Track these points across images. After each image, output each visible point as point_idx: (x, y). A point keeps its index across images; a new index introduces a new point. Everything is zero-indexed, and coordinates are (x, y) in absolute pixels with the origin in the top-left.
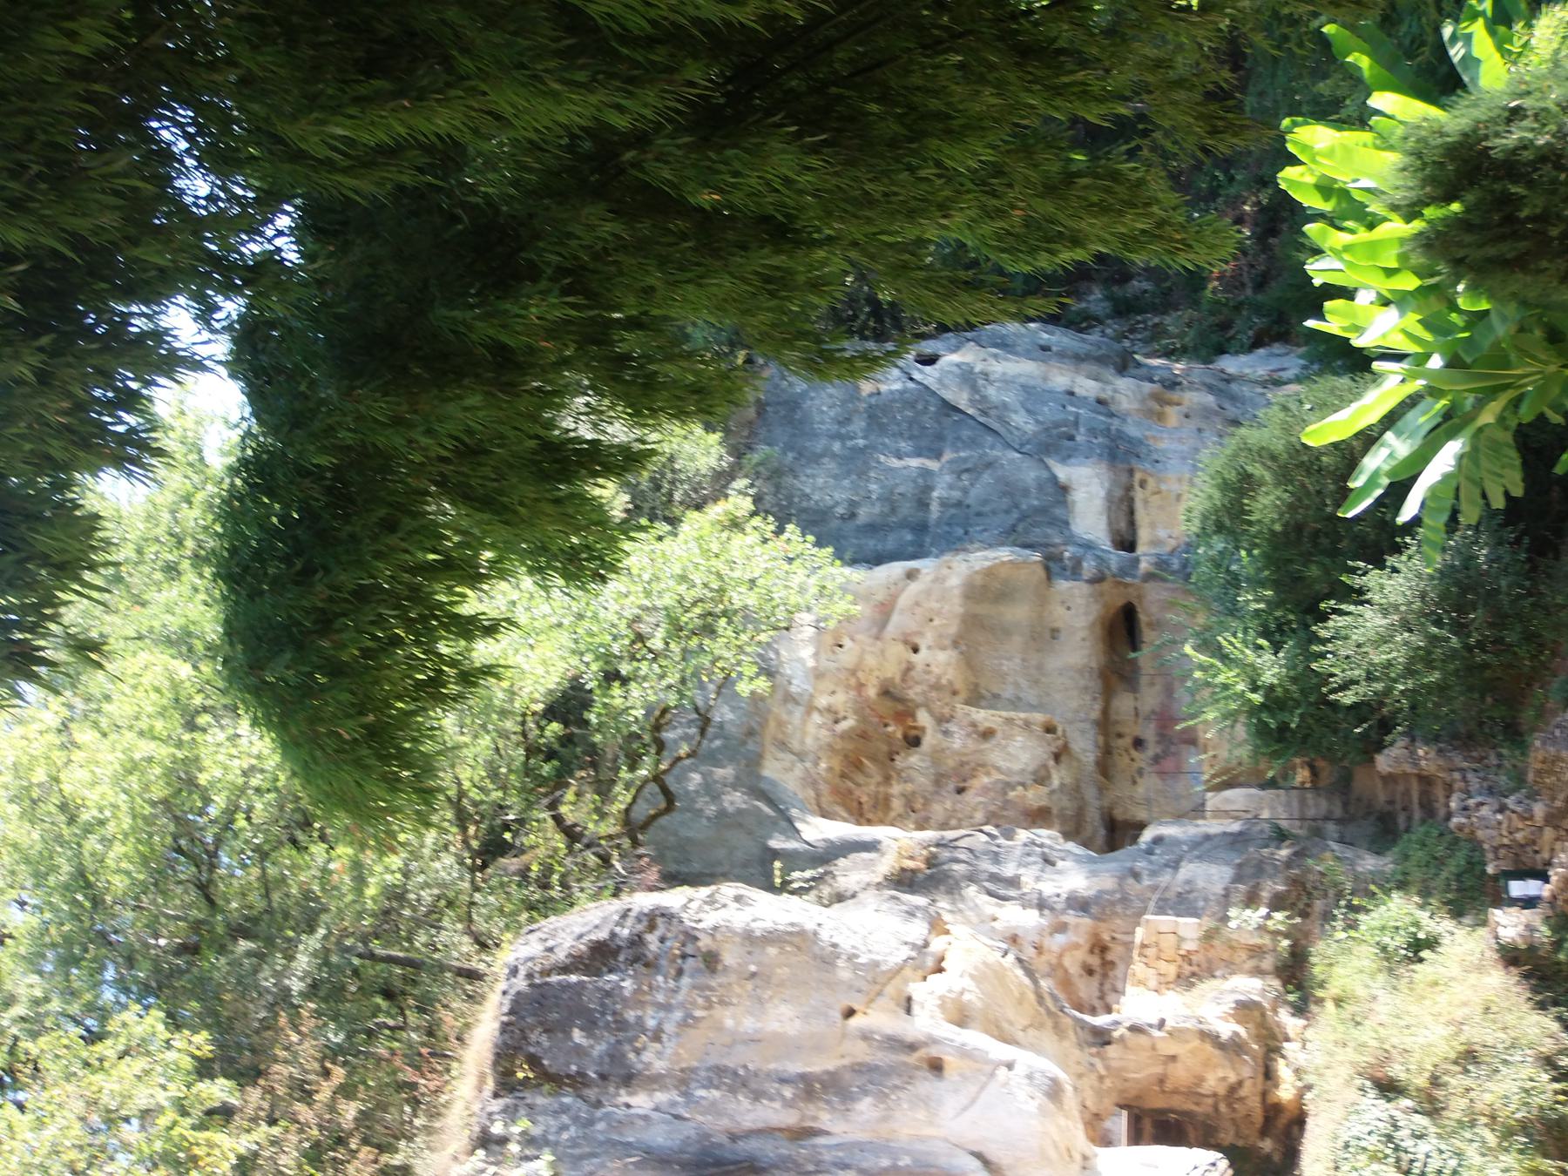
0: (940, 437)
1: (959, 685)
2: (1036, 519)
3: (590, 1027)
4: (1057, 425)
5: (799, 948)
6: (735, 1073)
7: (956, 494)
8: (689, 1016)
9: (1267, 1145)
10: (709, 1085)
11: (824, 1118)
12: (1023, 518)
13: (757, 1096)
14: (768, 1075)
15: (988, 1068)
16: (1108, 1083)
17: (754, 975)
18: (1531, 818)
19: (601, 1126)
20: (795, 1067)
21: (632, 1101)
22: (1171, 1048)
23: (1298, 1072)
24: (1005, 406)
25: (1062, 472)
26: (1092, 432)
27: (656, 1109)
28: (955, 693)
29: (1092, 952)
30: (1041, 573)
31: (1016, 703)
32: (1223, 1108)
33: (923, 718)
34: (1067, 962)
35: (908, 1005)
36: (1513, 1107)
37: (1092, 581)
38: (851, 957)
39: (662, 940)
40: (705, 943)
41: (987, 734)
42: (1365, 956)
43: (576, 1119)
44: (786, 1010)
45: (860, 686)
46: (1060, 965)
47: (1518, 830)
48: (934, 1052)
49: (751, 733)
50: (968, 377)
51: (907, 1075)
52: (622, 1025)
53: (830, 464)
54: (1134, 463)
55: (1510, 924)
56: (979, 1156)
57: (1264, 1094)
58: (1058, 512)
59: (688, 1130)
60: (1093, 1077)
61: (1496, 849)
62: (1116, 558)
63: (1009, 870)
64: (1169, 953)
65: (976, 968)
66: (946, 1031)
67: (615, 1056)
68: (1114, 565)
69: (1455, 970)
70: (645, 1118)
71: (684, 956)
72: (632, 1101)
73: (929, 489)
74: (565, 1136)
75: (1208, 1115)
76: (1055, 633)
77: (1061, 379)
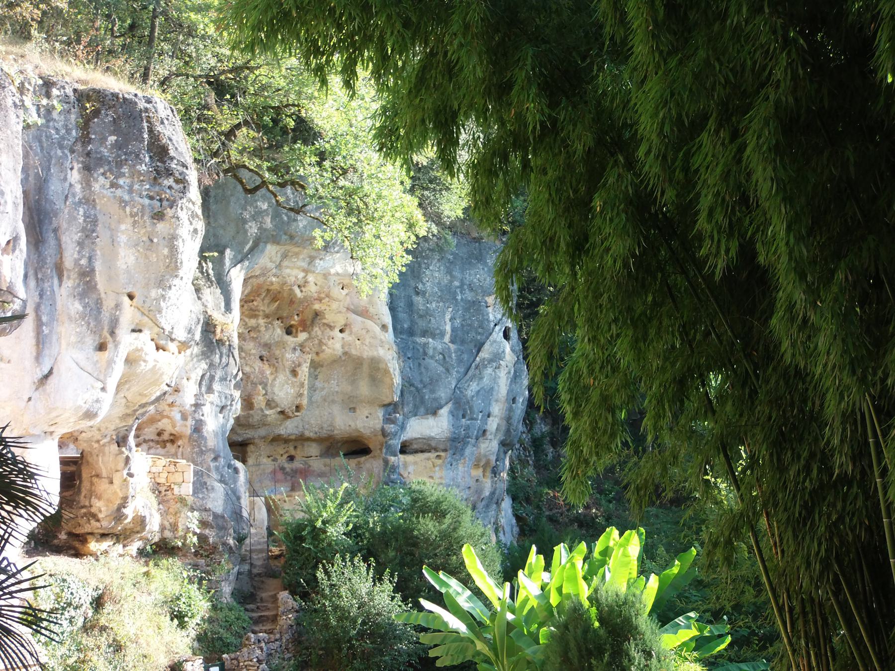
0: (463, 342)
1: (322, 356)
2: (417, 397)
3: (118, 146)
4: (471, 408)
6: (93, 231)
7: (431, 352)
8: (126, 203)
9: (63, 536)
10: (86, 216)
13: (80, 244)
14: (93, 250)
15: (102, 378)
16: (96, 445)
17: (152, 241)
19: (59, 152)
20: (98, 266)
21: (75, 171)
24: (481, 378)
25: (444, 411)
26: (467, 428)
27: (71, 185)
29: (171, 435)
30: (387, 401)
31: (312, 389)
32: (84, 510)
33: (303, 336)
34: (165, 421)
37: (383, 430)
39: (170, 187)
40: (169, 212)
41: (294, 373)
42: (174, 588)
44: (131, 260)
45: (320, 300)
46: (163, 417)
48: (110, 346)
49: (292, 237)
50: (497, 357)
51: (96, 331)
52: (120, 164)
53: (446, 280)
57: (92, 534)
58: (422, 410)
59: (59, 204)
60: (99, 437)
61: (236, 659)
62: (397, 443)
63: (216, 386)
64: (172, 479)
67: (101, 161)
70: (65, 179)
71: (161, 200)
72: (75, 171)
73: (433, 336)
75: (79, 502)
76: (353, 410)
77: (497, 409)
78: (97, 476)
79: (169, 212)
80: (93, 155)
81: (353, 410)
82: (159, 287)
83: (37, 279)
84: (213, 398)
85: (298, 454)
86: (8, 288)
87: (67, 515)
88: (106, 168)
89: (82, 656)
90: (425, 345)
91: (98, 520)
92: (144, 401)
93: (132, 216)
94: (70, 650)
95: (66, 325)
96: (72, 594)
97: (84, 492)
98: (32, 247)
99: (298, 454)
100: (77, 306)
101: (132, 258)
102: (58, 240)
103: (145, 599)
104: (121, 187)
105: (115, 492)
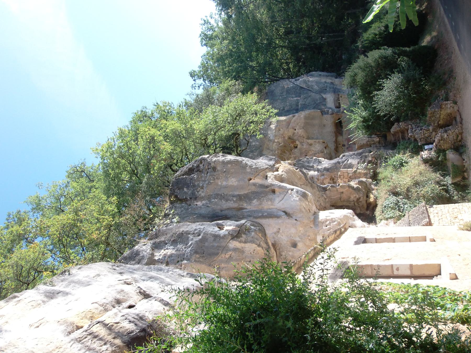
0: (300, 93)
1: (304, 136)
2: (319, 105)
3: (188, 187)
4: (323, 88)
6: (221, 195)
7: (304, 103)
8: (209, 182)
9: (368, 212)
10: (215, 198)
11: (245, 205)
13: (227, 200)
14: (230, 195)
16: (327, 200)
17: (225, 171)
18: (429, 130)
19: (189, 210)
20: (237, 193)
22: (342, 190)
24: (312, 85)
25: (324, 96)
26: (330, 88)
27: (203, 205)
28: (304, 137)
29: (330, 180)
31: (317, 139)
32: (356, 204)
33: (297, 142)
36: (429, 194)
37: (331, 114)
38: (251, 167)
39: (203, 165)
40: (212, 165)
41: (311, 145)
42: (390, 169)
43: (185, 209)
44: (233, 180)
45: (284, 137)
47: (426, 134)
48: (273, 188)
49: (261, 146)
50: (305, 82)
51: (266, 194)
52: (194, 186)
54: (339, 93)
56: (284, 212)
57: (366, 201)
58: (324, 103)
59: (210, 209)
60: (323, 198)
61: (420, 139)
62: (336, 110)
63: (311, 165)
64: (346, 176)
66: (277, 183)
67: (193, 193)
70: (200, 207)
73: (298, 103)
74: (182, 212)
76: (324, 126)
77: (323, 80)
78: (340, 199)
79: (212, 165)
84: (315, 166)
85: (342, 143)
86: (238, 227)
88: (195, 191)
92: (304, 179)
93: (214, 180)
95: (263, 206)
96: (391, 203)
101: (233, 179)
104: (203, 185)
105: (347, 191)
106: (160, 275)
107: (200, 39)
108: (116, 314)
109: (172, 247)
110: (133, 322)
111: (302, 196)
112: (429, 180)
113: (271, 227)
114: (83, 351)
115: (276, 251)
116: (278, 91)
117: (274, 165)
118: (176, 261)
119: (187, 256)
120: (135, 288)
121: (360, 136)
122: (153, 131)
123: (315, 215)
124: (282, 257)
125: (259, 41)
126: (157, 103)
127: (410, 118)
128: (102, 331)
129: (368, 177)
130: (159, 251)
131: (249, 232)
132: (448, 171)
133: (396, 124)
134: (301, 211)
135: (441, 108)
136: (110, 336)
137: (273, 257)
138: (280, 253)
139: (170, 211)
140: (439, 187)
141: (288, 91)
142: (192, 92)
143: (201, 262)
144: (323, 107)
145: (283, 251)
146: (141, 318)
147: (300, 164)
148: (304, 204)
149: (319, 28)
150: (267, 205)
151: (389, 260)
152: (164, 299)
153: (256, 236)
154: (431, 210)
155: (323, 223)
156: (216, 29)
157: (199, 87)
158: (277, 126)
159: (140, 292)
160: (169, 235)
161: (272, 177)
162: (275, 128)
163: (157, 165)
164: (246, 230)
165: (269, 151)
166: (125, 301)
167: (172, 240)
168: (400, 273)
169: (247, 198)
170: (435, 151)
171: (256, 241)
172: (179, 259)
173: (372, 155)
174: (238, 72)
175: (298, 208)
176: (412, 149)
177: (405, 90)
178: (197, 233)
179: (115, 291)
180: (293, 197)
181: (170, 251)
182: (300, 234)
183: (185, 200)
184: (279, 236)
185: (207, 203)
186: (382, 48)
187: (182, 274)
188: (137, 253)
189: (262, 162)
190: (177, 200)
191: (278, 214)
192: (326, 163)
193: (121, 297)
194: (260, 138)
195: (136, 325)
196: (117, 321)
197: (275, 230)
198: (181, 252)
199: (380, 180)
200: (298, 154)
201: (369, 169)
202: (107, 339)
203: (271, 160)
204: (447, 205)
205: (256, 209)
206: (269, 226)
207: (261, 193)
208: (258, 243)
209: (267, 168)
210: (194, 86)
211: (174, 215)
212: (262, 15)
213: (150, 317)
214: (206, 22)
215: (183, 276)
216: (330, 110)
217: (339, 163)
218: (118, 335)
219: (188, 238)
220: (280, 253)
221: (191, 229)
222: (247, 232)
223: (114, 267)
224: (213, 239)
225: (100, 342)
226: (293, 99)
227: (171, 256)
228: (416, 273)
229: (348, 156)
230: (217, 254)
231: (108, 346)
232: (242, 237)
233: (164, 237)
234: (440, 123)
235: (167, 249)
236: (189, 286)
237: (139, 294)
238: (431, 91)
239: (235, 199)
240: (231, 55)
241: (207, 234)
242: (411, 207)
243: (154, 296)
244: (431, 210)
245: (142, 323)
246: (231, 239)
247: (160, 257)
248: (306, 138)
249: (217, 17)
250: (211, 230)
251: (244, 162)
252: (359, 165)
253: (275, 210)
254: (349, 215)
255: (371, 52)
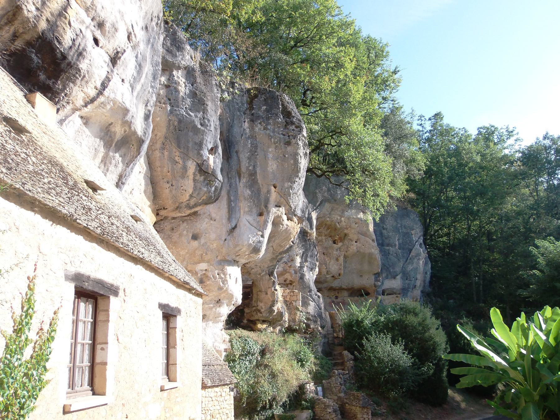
0: (403, 249)
1: (348, 252)
2: (388, 270)
3: (267, 111)
4: (409, 276)
5: (293, 170)
6: (256, 152)
7: (391, 253)
9: (245, 321)
11: (244, 180)
12: (388, 268)
13: (249, 158)
14: (256, 162)
15: (261, 229)
16: (259, 276)
19: (238, 113)
20: (258, 170)
21: (246, 124)
23: (265, 329)
24: (413, 264)
26: (409, 284)
28: (346, 252)
30: (376, 272)
31: (345, 267)
32: (254, 308)
33: (340, 244)
34: (288, 274)
35: (278, 206)
38: (291, 187)
39: (293, 130)
40: (293, 141)
41: (337, 260)
42: (297, 348)
46: (287, 272)
48: (265, 213)
49: (335, 201)
50: (418, 255)
52: (268, 119)
53: (395, 224)
55: (311, 387)
56: (236, 226)
57: (258, 320)
58: (390, 276)
59: (238, 138)
60: (260, 272)
61: (330, 383)
62: (380, 290)
63: (309, 259)
64: (292, 298)
65: (289, 230)
66: (271, 218)
67: (259, 117)
68: (379, 290)
69: (296, 372)
70: (241, 126)
71: (289, 136)
72: (246, 123)
74: (235, 104)
75: (252, 304)
76: (361, 276)
77: (419, 277)
78: (260, 291)
79: (293, 141)
80: (255, 115)
81: (361, 276)
82: (289, 181)
83: (228, 177)
85: (339, 295)
87: (247, 310)
88: (261, 120)
89: (256, 380)
90: (388, 250)
91: (261, 313)
92: (281, 250)
93: (275, 143)
94: (250, 377)
96: (250, 347)
97: (254, 299)
98: (225, 157)
99: (339, 295)
100: (248, 192)
101: (275, 166)
102: (238, 157)
103: (284, 352)
106: (146, 77)
107: (488, 125)
108: (83, 22)
109: (188, 92)
110: (74, 44)
111: (255, 247)
112: (278, 389)
113: (217, 211)
114: (316, 6)
115: (188, 215)
116: (407, 222)
117: (295, 215)
118: (170, 97)
119: (176, 110)
120: (123, 46)
121: (342, 317)
122: (350, 66)
123: (235, 262)
124: (181, 222)
125: (478, 199)
126: (398, 71)
127: (358, 373)
128: (56, 5)
129: (291, 323)
130: (184, 76)
131: (207, 184)
132: (289, 411)
133: (352, 357)
134: (237, 245)
135: (363, 407)
136: (49, 15)
137: (180, 212)
138: (186, 220)
139: (238, 89)
140: (269, 400)
141: (407, 235)
142: (415, 116)
143: (168, 127)
144: (384, 275)
145: (188, 224)
146: (80, 54)
147: (310, 246)
148: (244, 249)
149: (492, 273)
150: (244, 206)
151: (118, 340)
152: (110, 83)
153: (202, 193)
154: (226, 389)
155: (222, 270)
156: (499, 146)
157: (421, 125)
158: (361, 220)
159: (118, 52)
160: (203, 88)
161: (280, 213)
162: (358, 218)
163: (302, 72)
164: (210, 181)
165: (330, 210)
166: (103, 34)
167: (197, 92)
168: (98, 352)
169: (253, 183)
170: (313, 398)
171: (196, 193)
172: (172, 101)
173: (317, 328)
174: (436, 174)
175: (240, 243)
176: (320, 373)
177: (389, 369)
178: (205, 122)
179: (115, 21)
180: (257, 238)
181: (183, 88)
182: (208, 244)
183: (251, 108)
184: (206, 220)
185: (246, 134)
186: (448, 346)
187: (148, 105)
188: (180, 48)
189: (299, 200)
190: (252, 98)
191: (234, 219)
192: (311, 277)
193: (107, 29)
194: (345, 200)
195: (71, 47)
196: (72, 24)
197: (214, 215)
198: (181, 102)
199: (284, 336)
200: (326, 244)
201: (299, 325)
202: (45, 12)
203: (303, 212)
204: (233, 407)
205: (239, 193)
206: (219, 208)
207: (259, 200)
208: (194, 195)
209: (291, 207)
210: (423, 118)
211: (233, 94)
212: (510, 204)
213: (83, 65)
214: (510, 133)
215: (146, 106)
216: (379, 283)
217: (310, 291)
218: (53, 26)
219: (199, 112)
220: (186, 220)
221: (210, 115)
222: (206, 182)
223: (154, 19)
224: (197, 142)
225: (40, 3)
226: (396, 240)
227: (177, 91)
228: (97, 369)
229: (318, 302)
230: (179, 146)
231: (35, 13)
232: (201, 176)
233: (202, 82)
234: (347, 405)
235: (186, 86)
236: (131, 113)
237: (115, 51)
238: (388, 398)
239: (250, 168)
240: (460, 165)
241: (203, 135)
242: (246, 368)
243: (115, 70)
244: (226, 389)
245: (74, 55)
246: (197, 163)
247: (176, 78)
248: (346, 254)
249: (517, 147)
250: (209, 140)
251: (297, 179)
252: (304, 314)
253: (238, 216)
254: (235, 300)
255: (444, 333)
